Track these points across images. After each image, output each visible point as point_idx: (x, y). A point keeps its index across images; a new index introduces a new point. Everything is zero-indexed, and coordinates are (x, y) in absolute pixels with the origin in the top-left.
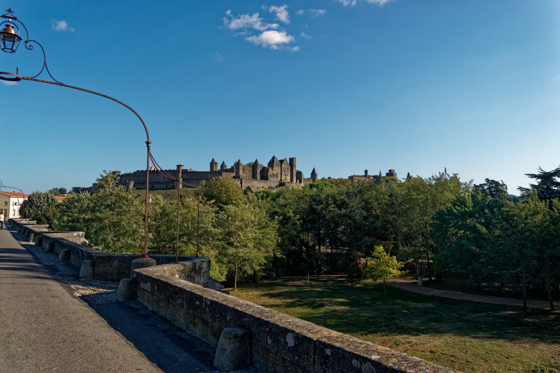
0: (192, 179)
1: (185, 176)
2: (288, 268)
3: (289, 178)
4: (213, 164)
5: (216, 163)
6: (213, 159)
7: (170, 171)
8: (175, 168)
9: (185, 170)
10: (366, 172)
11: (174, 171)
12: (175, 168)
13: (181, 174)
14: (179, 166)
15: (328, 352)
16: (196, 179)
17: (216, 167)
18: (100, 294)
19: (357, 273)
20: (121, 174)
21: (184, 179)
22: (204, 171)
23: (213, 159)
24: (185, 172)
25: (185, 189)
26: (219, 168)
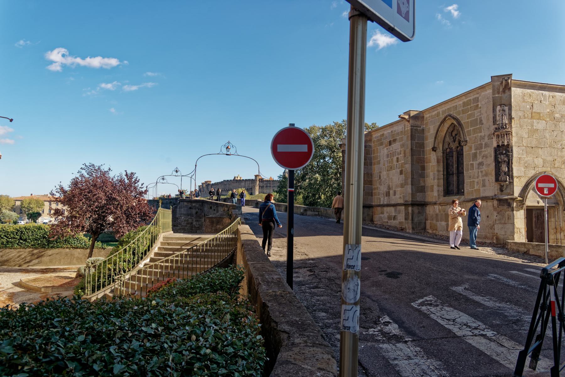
1: (261, 184)
7: (249, 180)
8: (254, 178)
13: (258, 182)
20: (211, 183)
24: (262, 180)
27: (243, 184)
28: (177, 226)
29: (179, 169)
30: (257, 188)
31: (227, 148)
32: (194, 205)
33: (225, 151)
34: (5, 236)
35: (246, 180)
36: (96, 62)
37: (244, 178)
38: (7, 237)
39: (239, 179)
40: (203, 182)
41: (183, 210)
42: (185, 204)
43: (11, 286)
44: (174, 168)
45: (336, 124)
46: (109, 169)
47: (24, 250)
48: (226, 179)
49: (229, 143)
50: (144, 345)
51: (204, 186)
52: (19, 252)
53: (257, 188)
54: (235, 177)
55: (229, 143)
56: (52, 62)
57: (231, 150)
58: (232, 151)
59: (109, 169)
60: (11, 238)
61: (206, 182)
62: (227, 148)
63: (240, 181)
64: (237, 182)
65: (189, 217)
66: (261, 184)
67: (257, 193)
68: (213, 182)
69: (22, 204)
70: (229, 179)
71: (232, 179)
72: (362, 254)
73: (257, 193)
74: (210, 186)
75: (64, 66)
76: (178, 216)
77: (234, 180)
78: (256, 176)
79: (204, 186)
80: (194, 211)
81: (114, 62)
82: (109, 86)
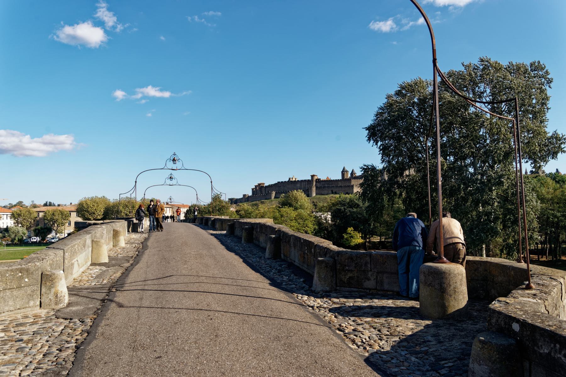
0: (324, 187)
1: (319, 185)
2: (447, 246)
3: (41, 370)
4: (344, 172)
5: (347, 171)
6: (344, 168)
7: (305, 181)
8: (310, 178)
9: (318, 179)
10: (557, 170)
11: (309, 180)
12: (310, 178)
13: (314, 183)
14: (313, 176)
15: (516, 327)
16: (328, 187)
17: (347, 174)
18: (343, 251)
19: (397, 129)
20: (265, 185)
21: (317, 187)
22: (335, 179)
23: (344, 168)
24: (318, 181)
25: (318, 196)
26: (349, 176)
27: (298, 185)
29: (179, 155)
30: (314, 189)
35: (302, 181)
39: (294, 180)
40: (257, 184)
43: (311, 226)
44: (169, 155)
45: (467, 67)
48: (280, 181)
50: (462, 169)
53: (314, 189)
54: (290, 179)
61: (259, 184)
66: (319, 185)
67: (314, 194)
68: (266, 184)
69: (45, 216)
70: (284, 180)
71: (287, 180)
72: (467, 261)
73: (314, 194)
74: (263, 189)
77: (288, 181)
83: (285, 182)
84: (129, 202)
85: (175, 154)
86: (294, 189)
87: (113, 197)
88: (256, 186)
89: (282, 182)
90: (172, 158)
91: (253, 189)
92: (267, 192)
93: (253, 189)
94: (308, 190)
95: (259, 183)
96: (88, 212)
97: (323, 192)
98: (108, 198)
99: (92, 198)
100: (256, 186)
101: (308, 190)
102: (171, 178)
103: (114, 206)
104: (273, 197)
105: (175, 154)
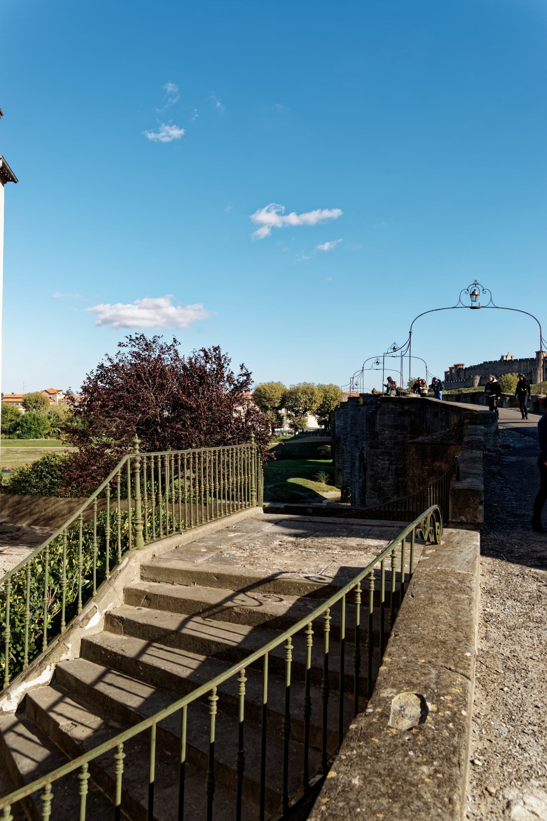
7: (527, 360)
8: (534, 356)
11: (532, 359)
12: (534, 356)
20: (464, 367)
27: (516, 366)
28: (378, 448)
31: (473, 294)
32: (407, 408)
33: (467, 300)
34: (48, 473)
35: (521, 360)
36: (313, 217)
37: (517, 356)
38: (52, 475)
39: (509, 358)
40: (452, 366)
41: (386, 417)
42: (391, 406)
46: (175, 341)
47: (76, 499)
48: (488, 360)
49: (476, 284)
51: (453, 371)
52: (69, 502)
54: (502, 357)
55: (476, 284)
56: (261, 225)
57: (479, 299)
58: (482, 300)
59: (175, 341)
60: (57, 478)
61: (456, 366)
62: (473, 294)
63: (512, 362)
64: (505, 365)
65: (399, 431)
68: (467, 366)
71: (498, 359)
74: (462, 372)
75: (274, 229)
76: (378, 428)
77: (500, 361)
78: (538, 353)
79: (453, 371)
80: (407, 420)
81: (336, 213)
82: (327, 246)
83: (495, 362)
84: (308, 388)
85: (395, 344)
86: (507, 373)
87: (290, 382)
88: (450, 368)
89: (490, 362)
90: (392, 347)
91: (446, 373)
92: (467, 377)
93: (446, 373)
94: (531, 373)
95: (456, 363)
96: (265, 398)
97: (158, 579)
98: (284, 384)
99: (336, 387)
100: (450, 368)
101: (531, 373)
102: (377, 362)
103: (291, 393)
104: (476, 385)
105: (395, 344)
